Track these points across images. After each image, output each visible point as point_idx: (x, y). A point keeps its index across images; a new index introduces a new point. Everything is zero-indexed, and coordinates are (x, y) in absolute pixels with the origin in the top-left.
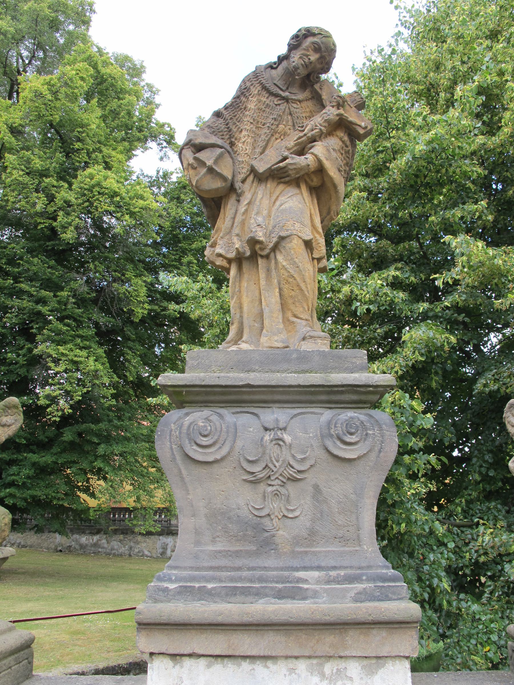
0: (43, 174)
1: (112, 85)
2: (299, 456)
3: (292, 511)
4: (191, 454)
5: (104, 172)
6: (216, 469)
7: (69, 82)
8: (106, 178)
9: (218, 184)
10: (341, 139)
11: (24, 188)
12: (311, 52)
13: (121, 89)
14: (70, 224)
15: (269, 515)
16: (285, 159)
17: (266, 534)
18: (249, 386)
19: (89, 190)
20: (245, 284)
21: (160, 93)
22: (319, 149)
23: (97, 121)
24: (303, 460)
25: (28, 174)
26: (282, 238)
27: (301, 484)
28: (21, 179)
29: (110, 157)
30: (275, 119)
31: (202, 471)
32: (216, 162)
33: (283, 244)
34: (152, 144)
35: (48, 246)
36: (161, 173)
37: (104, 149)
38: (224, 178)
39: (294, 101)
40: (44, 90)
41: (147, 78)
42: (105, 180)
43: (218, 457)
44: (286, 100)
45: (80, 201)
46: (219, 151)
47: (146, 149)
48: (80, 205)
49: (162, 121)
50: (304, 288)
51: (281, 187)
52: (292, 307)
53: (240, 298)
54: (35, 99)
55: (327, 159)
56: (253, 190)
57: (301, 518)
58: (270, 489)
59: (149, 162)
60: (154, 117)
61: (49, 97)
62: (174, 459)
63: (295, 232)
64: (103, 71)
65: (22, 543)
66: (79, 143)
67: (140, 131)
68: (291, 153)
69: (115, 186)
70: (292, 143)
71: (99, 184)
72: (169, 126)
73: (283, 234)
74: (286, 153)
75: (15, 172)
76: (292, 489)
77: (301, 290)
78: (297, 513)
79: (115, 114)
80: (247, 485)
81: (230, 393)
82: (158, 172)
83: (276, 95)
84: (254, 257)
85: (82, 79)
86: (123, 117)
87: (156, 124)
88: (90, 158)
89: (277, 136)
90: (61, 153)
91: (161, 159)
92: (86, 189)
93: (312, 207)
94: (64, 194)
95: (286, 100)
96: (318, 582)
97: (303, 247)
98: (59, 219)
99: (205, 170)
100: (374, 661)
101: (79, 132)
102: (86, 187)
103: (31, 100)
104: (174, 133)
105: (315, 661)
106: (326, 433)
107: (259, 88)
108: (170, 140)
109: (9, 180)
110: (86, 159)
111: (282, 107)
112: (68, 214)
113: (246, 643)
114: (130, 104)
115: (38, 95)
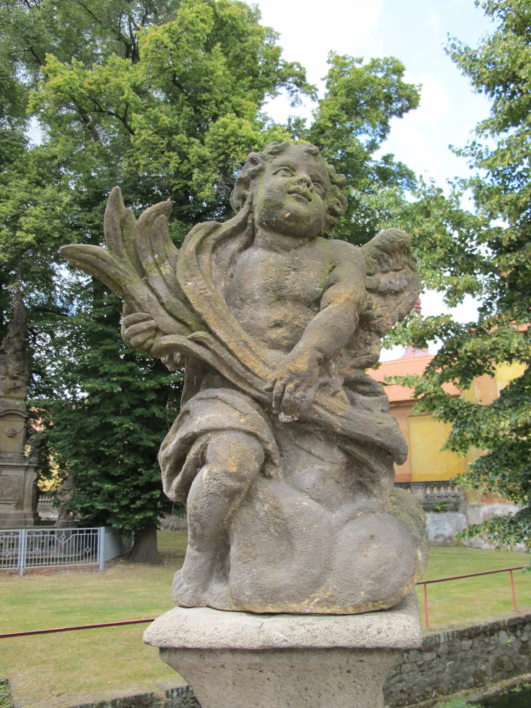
0: (171, 132)
1: (234, 27)
5: (237, 120)
7: (190, 26)
8: (240, 126)
11: (153, 149)
13: (243, 31)
14: (207, 181)
19: (223, 141)
21: (280, 37)
23: (223, 68)
25: (156, 133)
28: (150, 138)
29: (240, 106)
34: (282, 90)
35: (182, 211)
36: (293, 122)
37: (234, 99)
40: (166, 39)
41: (263, 23)
42: (240, 127)
45: (215, 155)
47: (276, 94)
48: (215, 159)
49: (289, 61)
54: (156, 50)
59: (279, 109)
60: (280, 58)
61: (171, 45)
64: (222, 13)
65: (175, 526)
66: (206, 94)
67: (267, 75)
69: (252, 134)
71: (234, 134)
72: (299, 65)
75: (143, 132)
79: (238, 59)
82: (289, 120)
85: (203, 21)
86: (248, 61)
87: (284, 66)
88: (219, 108)
90: (188, 106)
91: (293, 105)
92: (220, 141)
94: (196, 150)
98: (194, 177)
101: (205, 81)
102: (220, 138)
103: (153, 51)
104: (305, 72)
108: (301, 81)
109: (138, 142)
110: (215, 110)
112: (204, 171)
114: (255, 45)
115: (159, 45)
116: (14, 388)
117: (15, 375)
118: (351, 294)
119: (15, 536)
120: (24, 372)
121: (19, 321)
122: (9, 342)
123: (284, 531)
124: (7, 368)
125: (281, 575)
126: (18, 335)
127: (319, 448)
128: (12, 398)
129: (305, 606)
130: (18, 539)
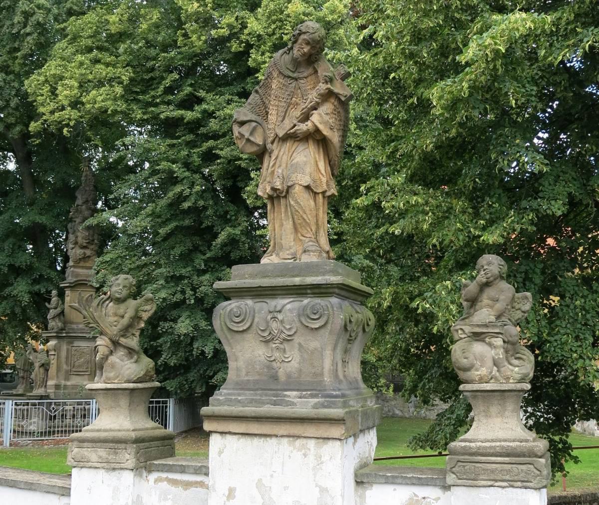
2: (288, 327)
3: (288, 358)
4: (231, 327)
6: (245, 335)
9: (254, 149)
10: (333, 104)
12: (304, 46)
15: (274, 360)
16: (295, 126)
17: (273, 371)
18: (260, 287)
20: (276, 214)
22: (315, 118)
24: (290, 329)
26: (289, 187)
27: (291, 343)
30: (289, 95)
31: (238, 336)
32: (251, 134)
33: (290, 191)
38: (258, 145)
39: (301, 78)
43: (245, 328)
44: (296, 79)
46: (254, 124)
50: (305, 218)
51: (296, 144)
52: (300, 230)
53: (274, 224)
55: (321, 123)
56: (278, 149)
57: (292, 362)
58: (274, 346)
62: (222, 330)
63: (296, 182)
68: (299, 122)
70: (299, 114)
73: (290, 184)
74: (295, 122)
76: (286, 346)
77: (304, 219)
78: (290, 359)
80: (263, 343)
81: (253, 291)
83: (289, 77)
84: (278, 197)
89: (292, 106)
93: (317, 156)
95: (296, 79)
96: (295, 397)
97: (303, 190)
99: (244, 141)
100: (321, 440)
105: (291, 439)
106: (302, 313)
107: (277, 73)
111: (293, 85)
113: (254, 428)
116: (84, 258)
117: (85, 244)
118: (224, 270)
119: (87, 407)
120: (93, 240)
121: (88, 189)
122: (77, 211)
123: (113, 366)
124: (77, 237)
125: (112, 375)
126: (86, 202)
127: (122, 349)
128: (83, 267)
129: (116, 381)
130: (89, 410)
